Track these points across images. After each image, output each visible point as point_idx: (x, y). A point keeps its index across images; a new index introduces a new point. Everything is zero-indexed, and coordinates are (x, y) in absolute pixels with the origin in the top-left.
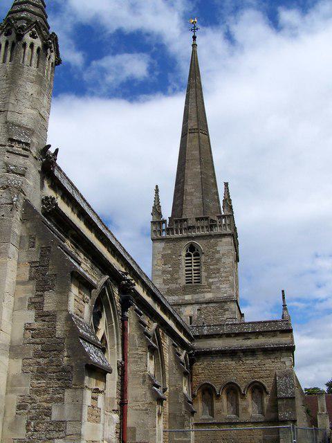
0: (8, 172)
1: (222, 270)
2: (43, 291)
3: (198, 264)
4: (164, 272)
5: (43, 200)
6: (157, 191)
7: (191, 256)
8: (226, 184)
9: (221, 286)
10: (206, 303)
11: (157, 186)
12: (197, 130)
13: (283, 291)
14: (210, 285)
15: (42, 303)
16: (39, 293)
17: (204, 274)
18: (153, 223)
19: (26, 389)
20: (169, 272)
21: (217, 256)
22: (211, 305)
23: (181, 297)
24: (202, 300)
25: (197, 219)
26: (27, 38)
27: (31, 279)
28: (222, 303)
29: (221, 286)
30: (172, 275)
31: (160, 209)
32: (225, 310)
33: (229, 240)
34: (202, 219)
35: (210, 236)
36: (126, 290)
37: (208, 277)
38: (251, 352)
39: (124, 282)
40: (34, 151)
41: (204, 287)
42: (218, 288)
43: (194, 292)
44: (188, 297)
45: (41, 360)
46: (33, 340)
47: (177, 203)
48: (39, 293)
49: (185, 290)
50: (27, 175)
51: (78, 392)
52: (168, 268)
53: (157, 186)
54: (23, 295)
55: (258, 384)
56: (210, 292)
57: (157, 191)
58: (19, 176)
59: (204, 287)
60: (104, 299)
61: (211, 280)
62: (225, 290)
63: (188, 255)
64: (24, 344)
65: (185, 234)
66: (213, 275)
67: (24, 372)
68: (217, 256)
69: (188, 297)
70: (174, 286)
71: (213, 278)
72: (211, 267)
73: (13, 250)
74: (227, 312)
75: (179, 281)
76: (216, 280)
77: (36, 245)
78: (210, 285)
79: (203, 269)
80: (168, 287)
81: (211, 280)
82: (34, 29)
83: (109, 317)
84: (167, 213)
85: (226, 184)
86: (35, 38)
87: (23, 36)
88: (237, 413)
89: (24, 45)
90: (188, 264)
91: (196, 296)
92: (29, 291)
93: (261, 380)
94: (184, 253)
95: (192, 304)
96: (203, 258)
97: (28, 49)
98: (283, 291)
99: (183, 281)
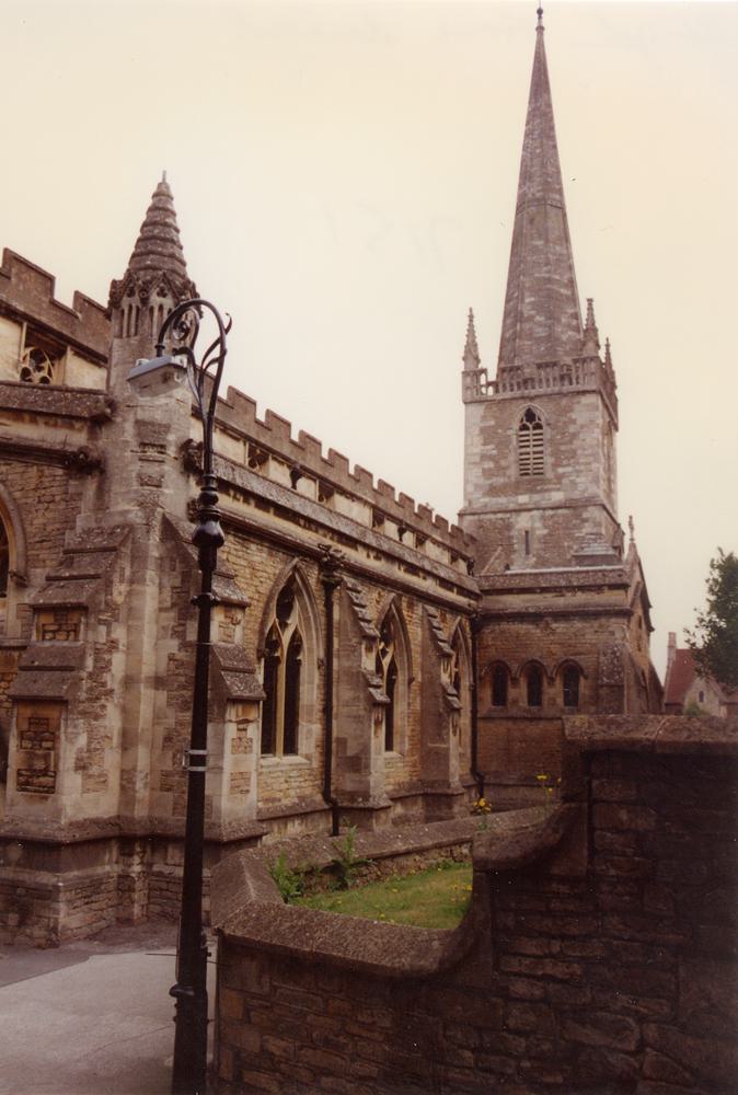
0: (142, 485)
1: (579, 452)
2: (186, 620)
3: (539, 442)
4: (484, 457)
5: (188, 505)
6: (471, 317)
7: (528, 429)
8: (590, 301)
9: (578, 480)
10: (552, 509)
11: (471, 310)
12: (541, 202)
13: (631, 517)
14: (559, 478)
15: (184, 632)
16: (182, 622)
17: (549, 460)
18: (465, 374)
19: (171, 721)
20: (491, 458)
21: (572, 429)
22: (560, 511)
23: (512, 499)
24: (544, 504)
25: (539, 366)
26: (155, 300)
27: (174, 605)
28: (575, 506)
29: (578, 480)
30: (497, 462)
31: (476, 350)
32: (586, 520)
33: (594, 399)
34: (547, 365)
35: (560, 394)
36: (329, 565)
37: (556, 465)
38: (563, 615)
39: (325, 559)
40: (172, 451)
41: (549, 481)
42: (574, 483)
43: (532, 491)
44: (523, 499)
45: (184, 692)
46: (177, 671)
47: (507, 335)
48: (182, 622)
49: (516, 488)
50: (163, 485)
51: (220, 726)
52: (491, 449)
53: (471, 310)
54: (166, 623)
55: (571, 663)
56: (559, 490)
57: (471, 317)
58: (155, 489)
59: (549, 481)
60: (295, 586)
61: (560, 470)
62: (584, 486)
63: (524, 428)
64: (169, 675)
65: (517, 393)
66: (565, 462)
67: (169, 704)
68: (572, 429)
69: (523, 499)
70: (501, 480)
71: (564, 466)
72: (563, 448)
73: (151, 574)
74: (586, 524)
75: (508, 472)
76: (570, 469)
77: (178, 569)
78: (559, 478)
79: (548, 450)
80: (489, 482)
81: (560, 470)
82: (162, 285)
83: (304, 608)
84: (490, 360)
85: (590, 301)
86: (164, 296)
87: (147, 298)
88: (483, 719)
89: (152, 309)
90: (523, 444)
91: (536, 497)
92: (170, 618)
93: (577, 658)
94: (516, 426)
95: (530, 510)
96: (547, 432)
97: (156, 313)
98: (631, 517)
99: (513, 472)
